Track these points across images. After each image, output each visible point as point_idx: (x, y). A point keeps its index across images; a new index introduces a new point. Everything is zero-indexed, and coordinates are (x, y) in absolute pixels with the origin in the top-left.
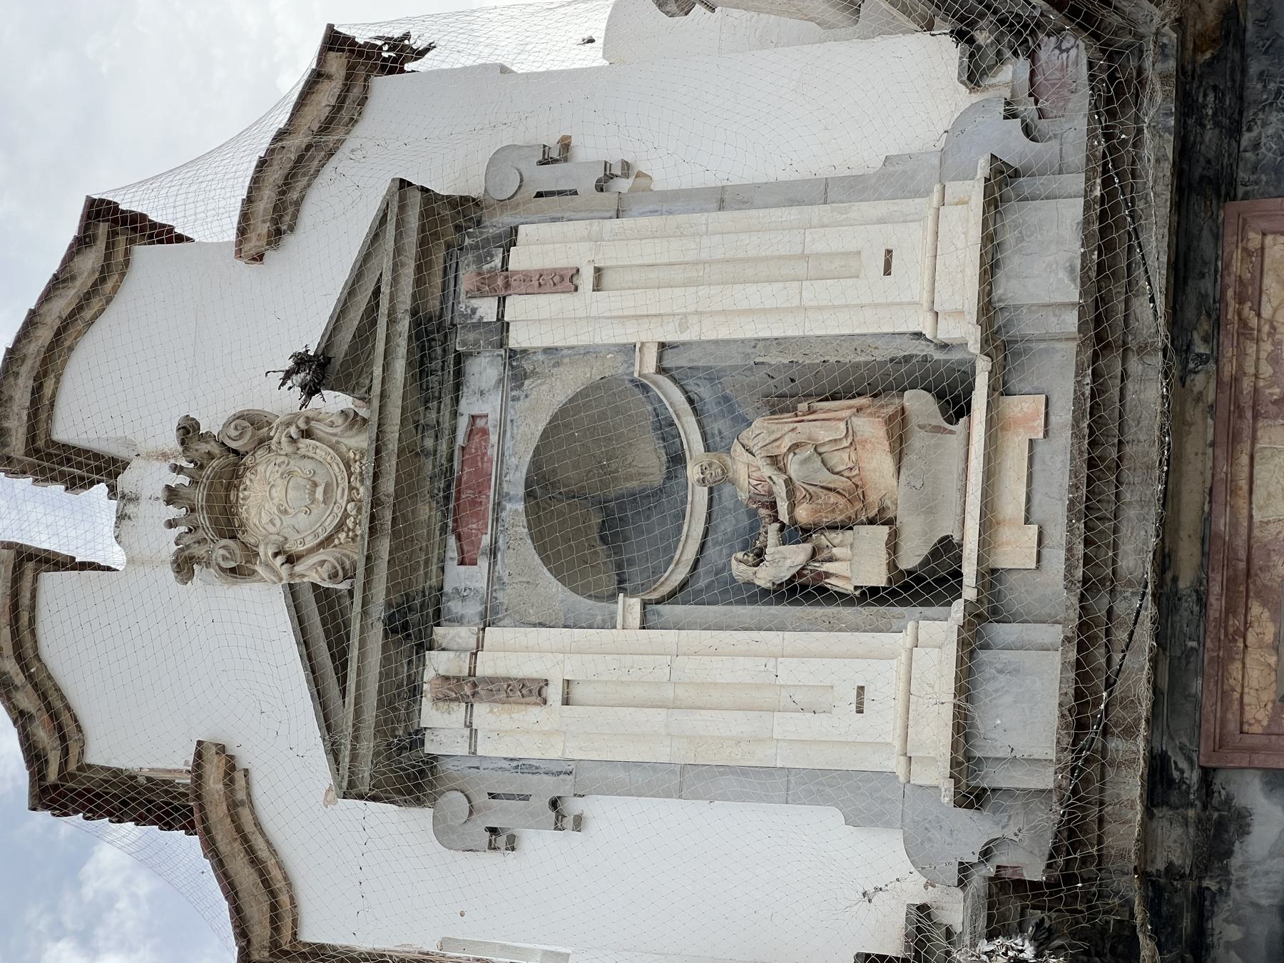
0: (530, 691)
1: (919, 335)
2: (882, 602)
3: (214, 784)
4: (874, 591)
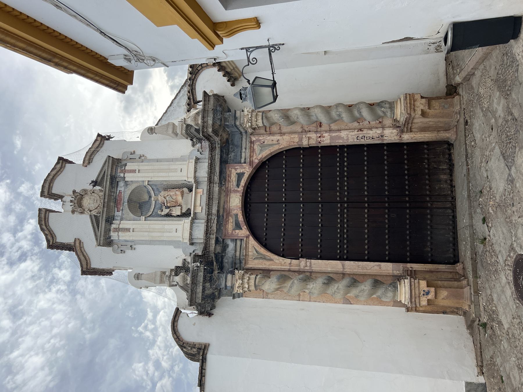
0: (128, 230)
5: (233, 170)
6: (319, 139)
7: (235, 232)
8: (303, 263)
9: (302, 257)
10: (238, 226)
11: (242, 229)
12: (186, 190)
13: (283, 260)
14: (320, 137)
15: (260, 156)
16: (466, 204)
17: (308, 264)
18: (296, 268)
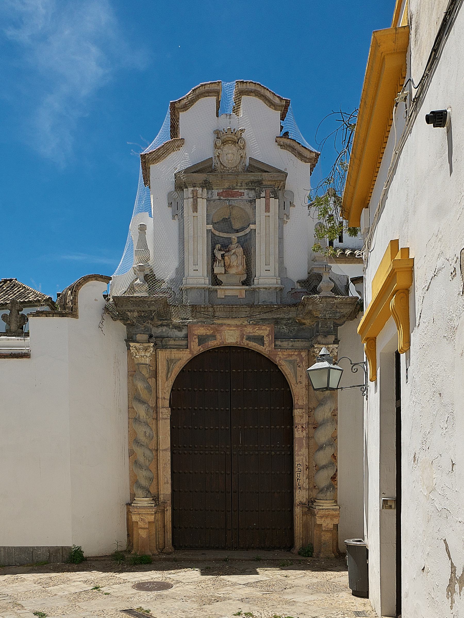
0: (195, 209)
1: (255, 276)
2: (212, 272)
3: (178, 143)
4: (214, 270)
5: (267, 332)
6: (300, 427)
7: (195, 338)
8: (165, 413)
9: (172, 410)
10: (202, 340)
11: (199, 345)
12: (244, 277)
13: (168, 391)
14: (302, 427)
15: (283, 363)
16: (191, 243)
17: (165, 416)
18: (160, 405)
